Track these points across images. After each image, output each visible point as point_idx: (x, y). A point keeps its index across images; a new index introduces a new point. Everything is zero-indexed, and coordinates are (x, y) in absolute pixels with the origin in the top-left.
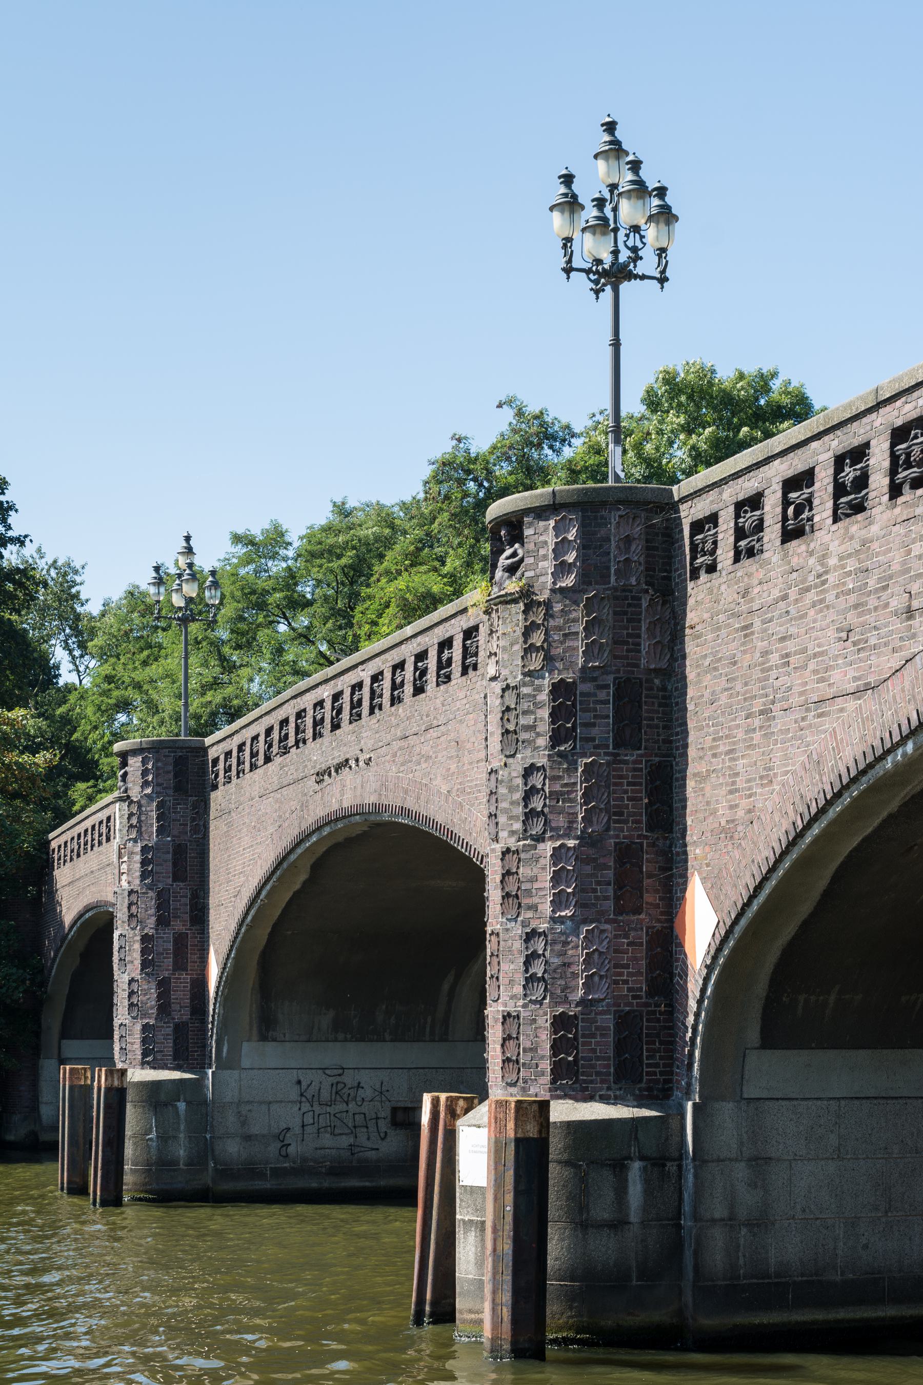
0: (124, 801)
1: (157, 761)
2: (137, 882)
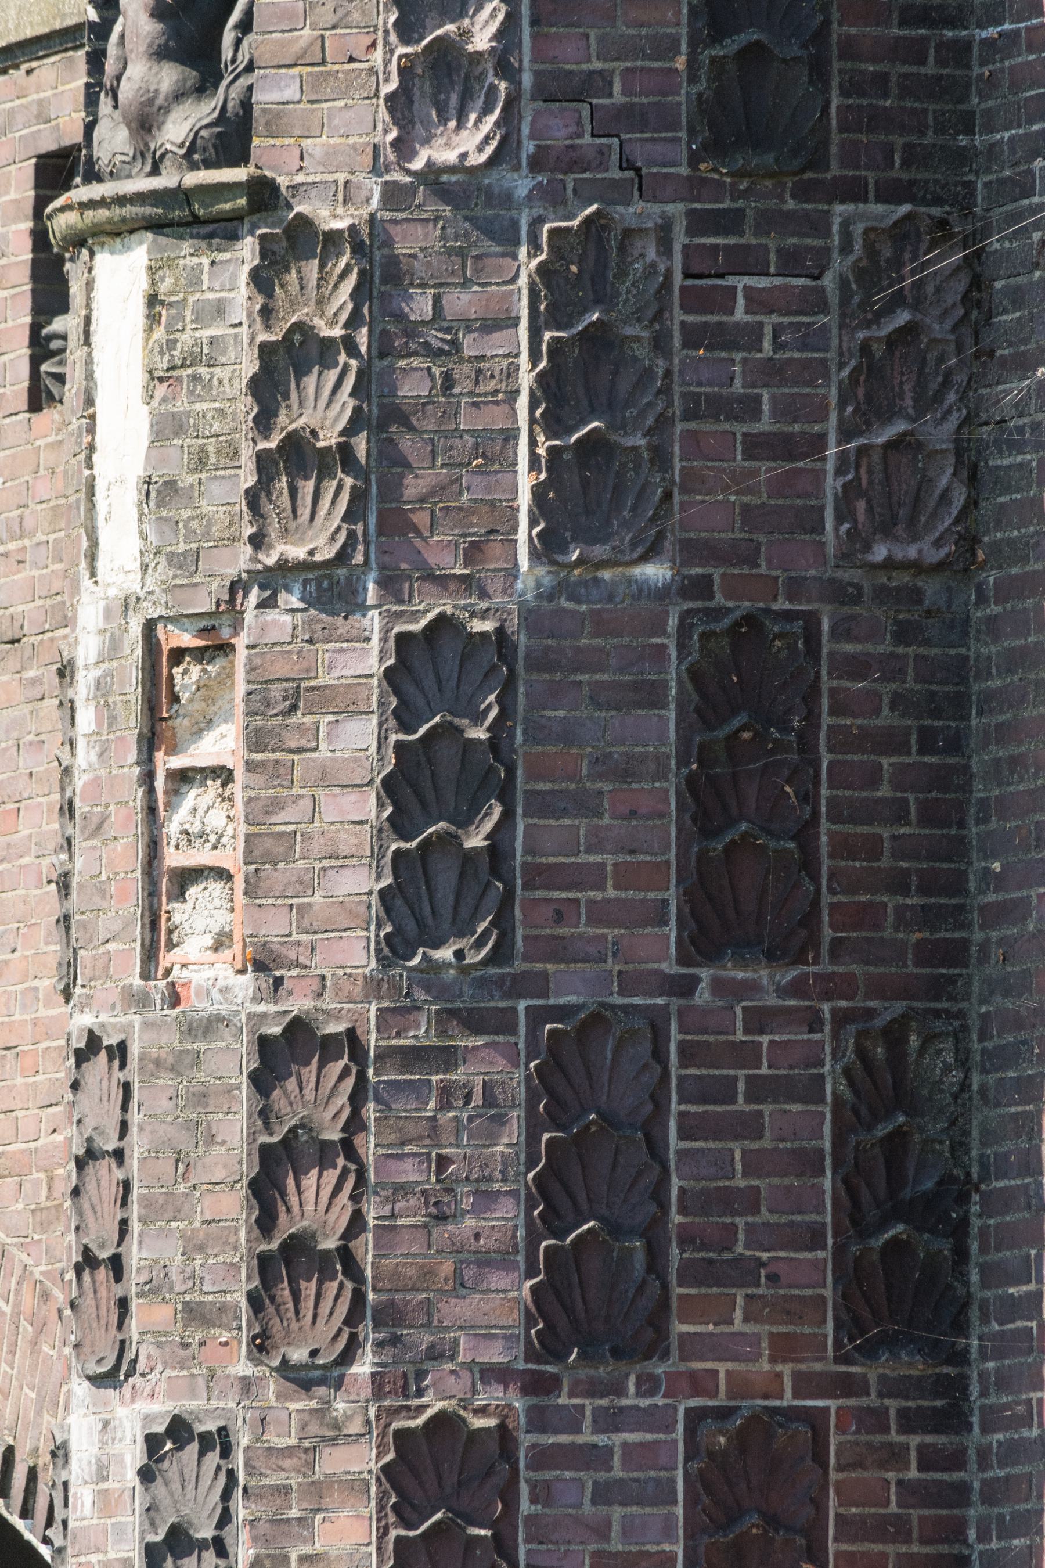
0: (221, 230)
2: (355, 953)
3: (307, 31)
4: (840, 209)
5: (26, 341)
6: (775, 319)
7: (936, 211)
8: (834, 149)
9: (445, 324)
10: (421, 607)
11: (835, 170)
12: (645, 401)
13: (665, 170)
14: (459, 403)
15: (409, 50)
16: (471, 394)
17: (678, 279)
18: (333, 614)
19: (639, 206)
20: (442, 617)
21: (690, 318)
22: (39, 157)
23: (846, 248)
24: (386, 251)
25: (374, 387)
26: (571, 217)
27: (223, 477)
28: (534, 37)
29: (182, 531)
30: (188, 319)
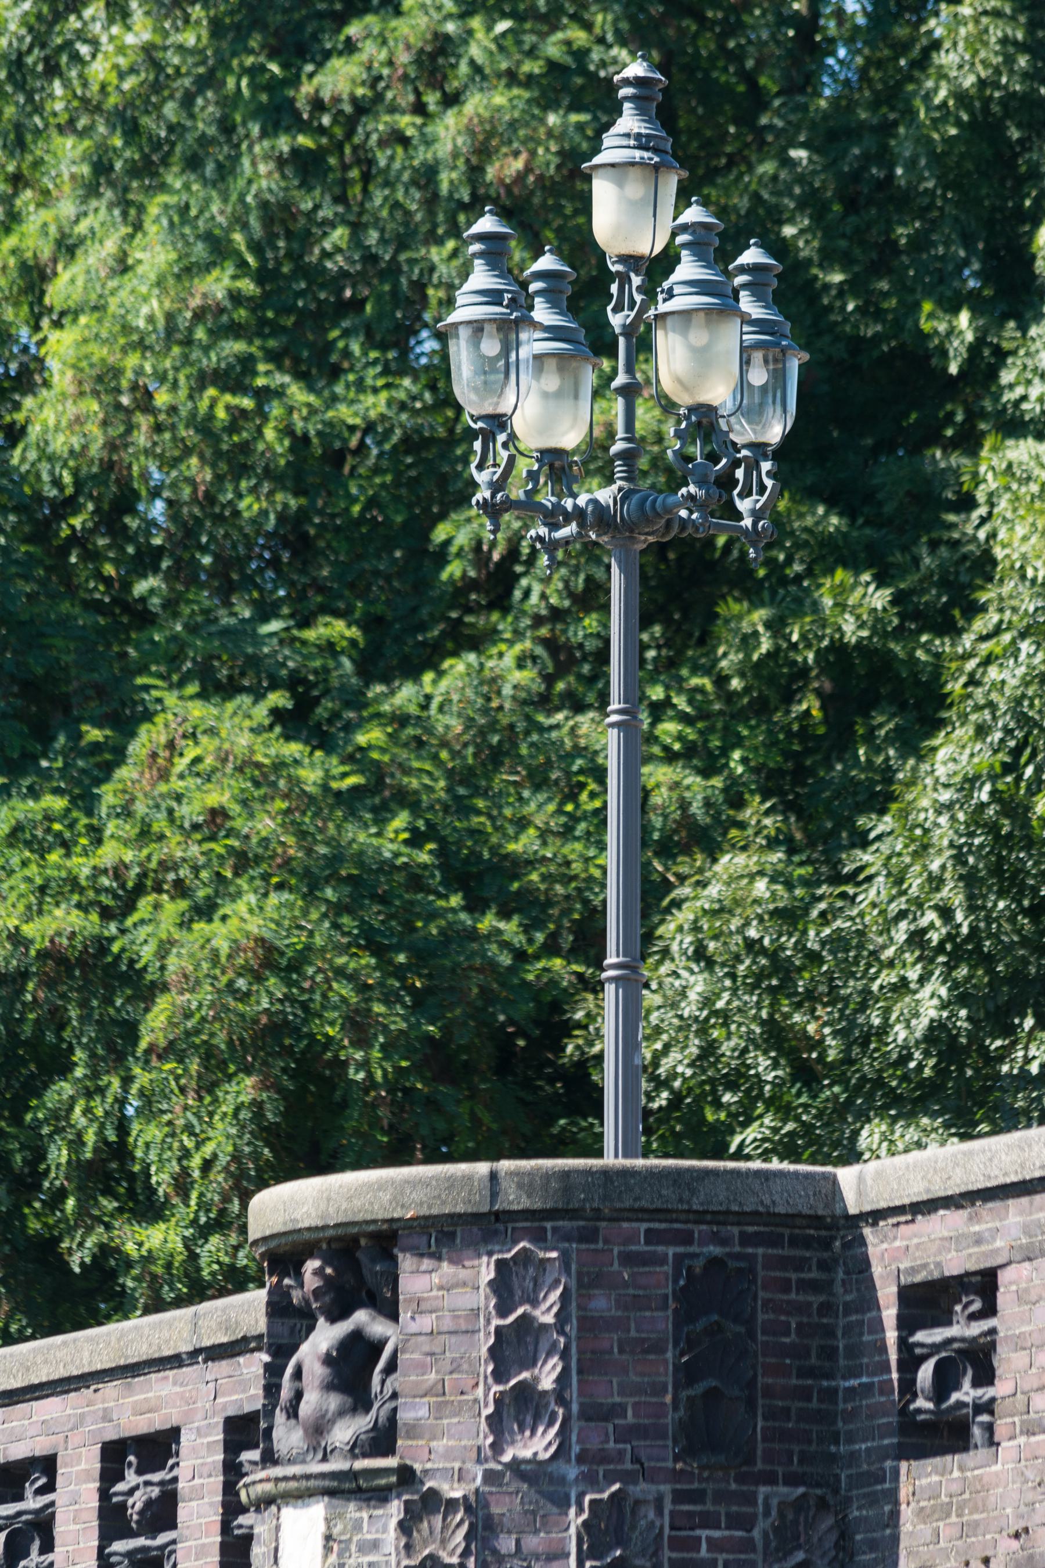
0: (379, 1496)
1: (586, 1283)
4: (763, 1490)
6: (725, 1556)
7: (819, 1492)
8: (759, 1453)
11: (760, 1466)
17: (667, 1531)
21: (674, 1555)
23: (767, 1513)
26: (602, 1491)
28: (579, 1381)
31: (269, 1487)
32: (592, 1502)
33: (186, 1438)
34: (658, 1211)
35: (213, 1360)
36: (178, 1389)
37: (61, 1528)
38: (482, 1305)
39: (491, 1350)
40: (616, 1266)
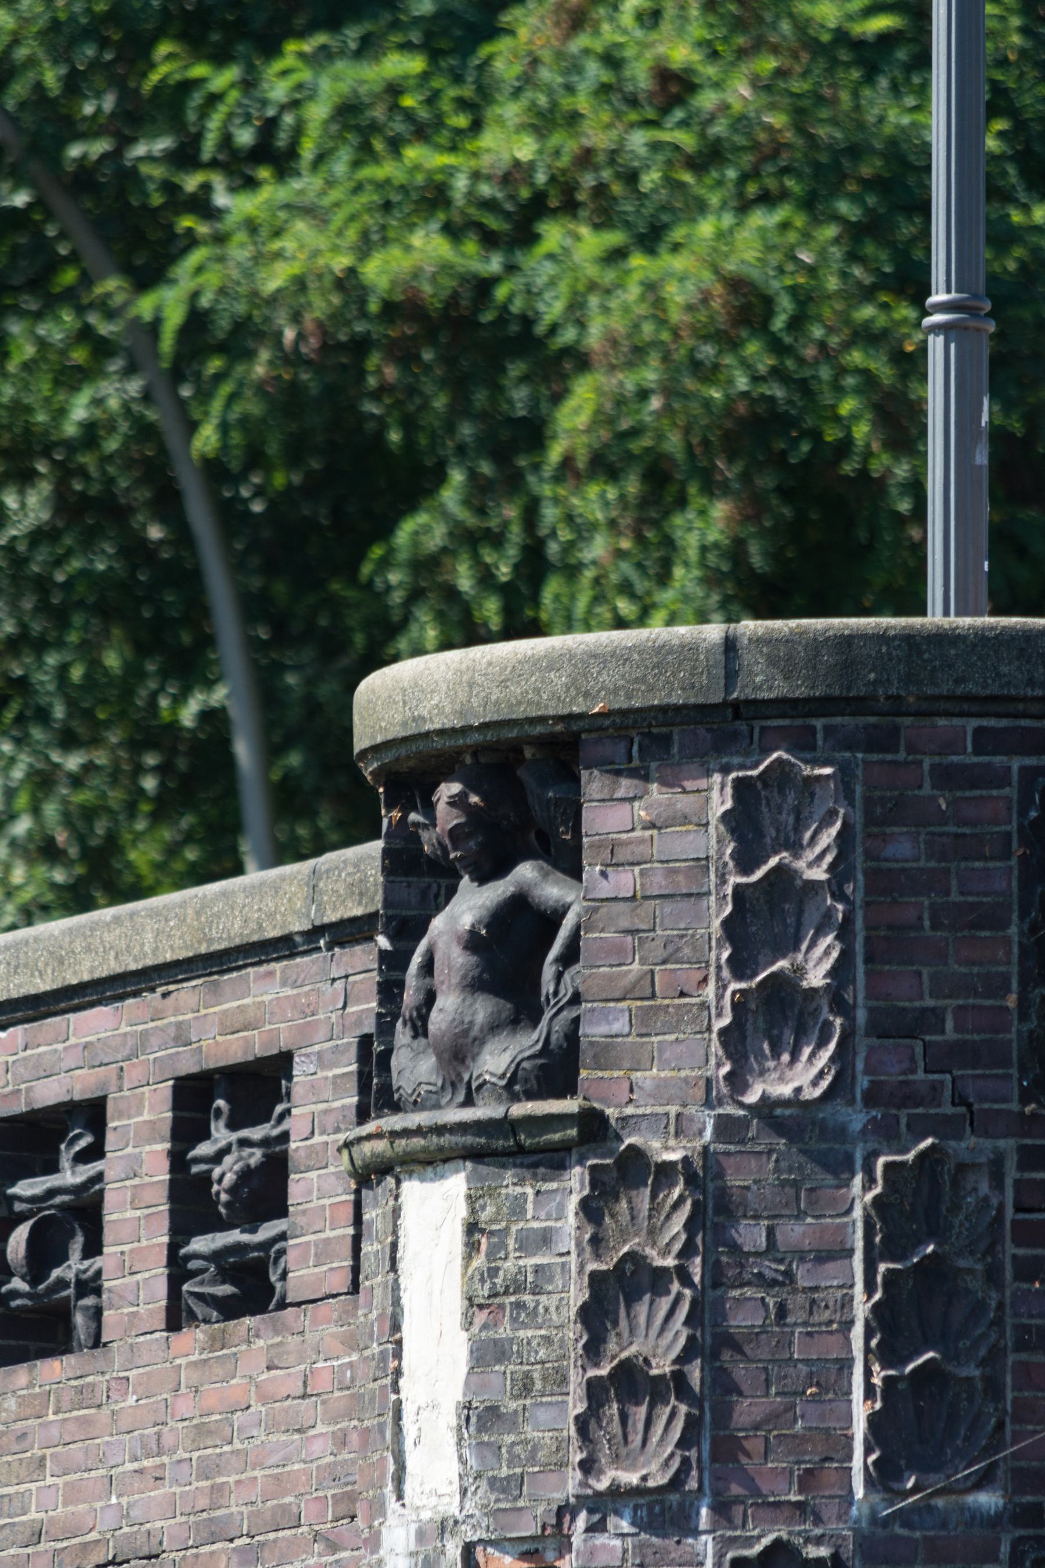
0: (551, 1160)
1: (876, 819)
3: (636, 966)
5: (164, 1260)
9: (779, 1256)
10: (756, 1533)
12: (979, 1332)
13: (996, 1106)
14: (793, 1333)
15: (743, 985)
16: (805, 1324)
17: (1009, 1212)
18: (665, 1536)
19: (972, 1141)
20: (777, 1543)
21: (1021, 1252)
22: (177, 1079)
24: (719, 1183)
25: (707, 1316)
26: (905, 1150)
27: (550, 1404)
28: (868, 974)
29: (505, 1456)
30: (511, 1247)
31: (380, 1146)
32: (888, 1166)
33: (301, 1069)
34: (994, 699)
35: (342, 944)
36: (290, 992)
37: (117, 1213)
38: (712, 852)
39: (726, 924)
40: (927, 790)
